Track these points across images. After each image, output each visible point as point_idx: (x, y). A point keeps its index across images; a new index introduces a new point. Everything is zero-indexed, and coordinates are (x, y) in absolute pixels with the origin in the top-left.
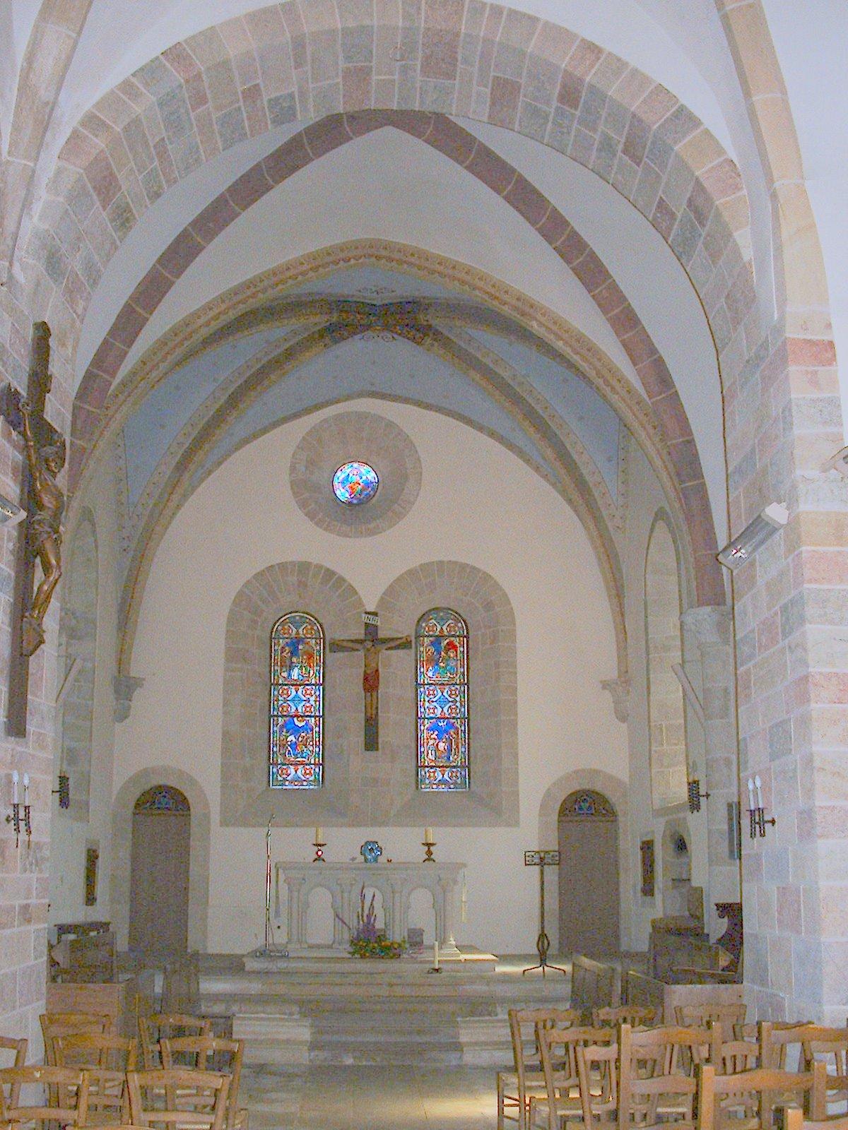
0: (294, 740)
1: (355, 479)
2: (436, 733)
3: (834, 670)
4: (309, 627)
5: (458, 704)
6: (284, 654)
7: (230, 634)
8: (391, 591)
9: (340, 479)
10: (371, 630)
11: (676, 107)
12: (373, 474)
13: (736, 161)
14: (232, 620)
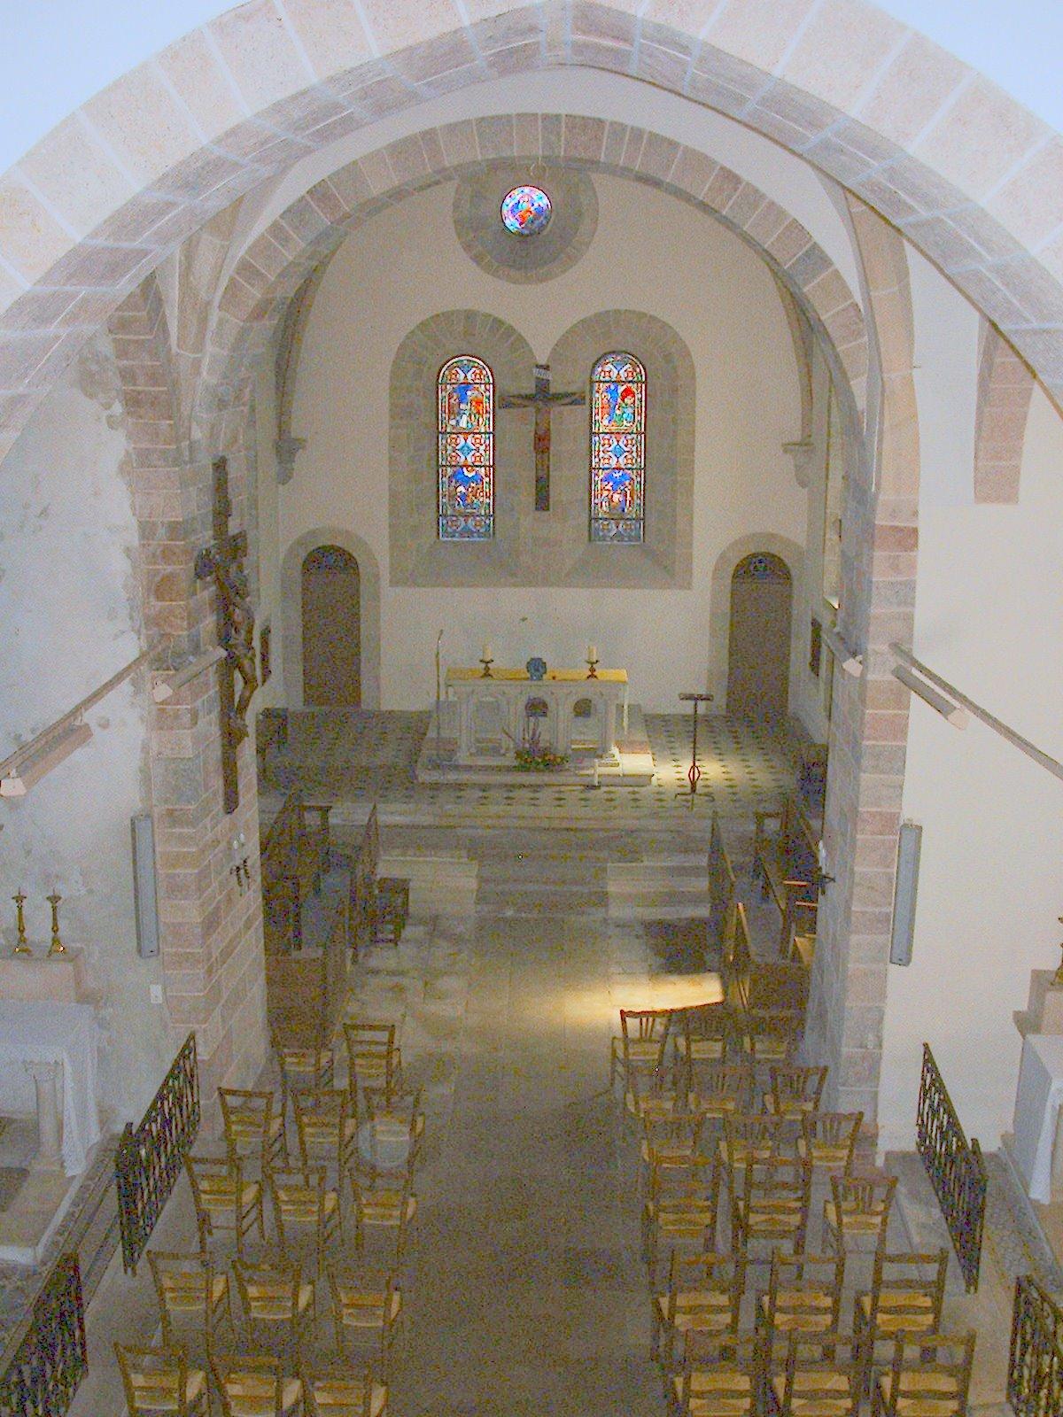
0: (464, 491)
1: (525, 206)
2: (611, 484)
3: (879, 810)
4: (478, 372)
5: (634, 454)
6: (452, 401)
7: (393, 389)
8: (564, 342)
9: (510, 205)
10: (543, 386)
11: (808, 246)
12: (545, 201)
13: (861, 307)
14: (397, 373)
